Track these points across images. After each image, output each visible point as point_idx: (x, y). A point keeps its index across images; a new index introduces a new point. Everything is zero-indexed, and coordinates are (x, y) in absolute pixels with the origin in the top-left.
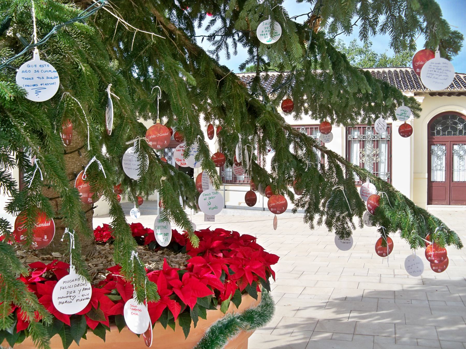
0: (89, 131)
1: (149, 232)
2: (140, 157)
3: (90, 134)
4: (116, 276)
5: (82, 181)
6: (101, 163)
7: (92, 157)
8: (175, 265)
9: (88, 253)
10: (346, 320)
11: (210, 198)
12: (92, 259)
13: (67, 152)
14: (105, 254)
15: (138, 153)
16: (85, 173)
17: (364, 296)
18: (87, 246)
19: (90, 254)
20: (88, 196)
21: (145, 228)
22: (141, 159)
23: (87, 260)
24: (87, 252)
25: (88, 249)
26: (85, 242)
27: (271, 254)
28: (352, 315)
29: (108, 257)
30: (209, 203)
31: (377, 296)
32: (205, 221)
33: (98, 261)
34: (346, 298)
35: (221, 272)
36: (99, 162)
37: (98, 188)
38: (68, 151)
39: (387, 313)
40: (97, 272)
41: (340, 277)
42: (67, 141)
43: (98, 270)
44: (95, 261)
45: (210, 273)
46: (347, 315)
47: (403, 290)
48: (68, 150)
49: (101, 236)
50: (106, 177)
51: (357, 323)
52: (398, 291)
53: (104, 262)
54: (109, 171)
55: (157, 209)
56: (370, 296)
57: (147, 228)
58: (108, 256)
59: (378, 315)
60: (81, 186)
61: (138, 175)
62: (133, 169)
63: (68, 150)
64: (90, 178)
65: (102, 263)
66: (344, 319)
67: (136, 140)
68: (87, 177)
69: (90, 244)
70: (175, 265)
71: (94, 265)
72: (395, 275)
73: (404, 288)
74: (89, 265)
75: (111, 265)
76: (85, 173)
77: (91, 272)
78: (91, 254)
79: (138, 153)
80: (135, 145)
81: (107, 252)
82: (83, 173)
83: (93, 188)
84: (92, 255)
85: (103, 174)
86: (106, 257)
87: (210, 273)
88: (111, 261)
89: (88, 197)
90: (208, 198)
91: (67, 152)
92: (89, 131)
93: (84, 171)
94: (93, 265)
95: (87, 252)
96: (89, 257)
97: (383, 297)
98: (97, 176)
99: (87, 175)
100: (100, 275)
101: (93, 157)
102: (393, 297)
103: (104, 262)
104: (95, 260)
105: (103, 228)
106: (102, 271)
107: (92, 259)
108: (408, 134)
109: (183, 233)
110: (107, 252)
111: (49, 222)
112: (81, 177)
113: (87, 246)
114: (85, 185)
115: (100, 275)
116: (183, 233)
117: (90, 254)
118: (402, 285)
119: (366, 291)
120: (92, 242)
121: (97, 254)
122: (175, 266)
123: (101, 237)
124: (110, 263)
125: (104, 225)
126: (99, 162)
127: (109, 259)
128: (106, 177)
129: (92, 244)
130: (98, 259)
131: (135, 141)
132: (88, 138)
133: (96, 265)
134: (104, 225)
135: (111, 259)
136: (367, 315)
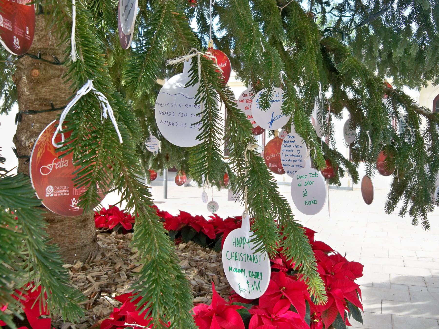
0: (74, 8)
1: (166, 217)
2: (202, 95)
3: (77, 17)
4: (132, 326)
5: (52, 151)
6: (108, 99)
7: (82, 83)
8: (212, 274)
9: (87, 255)
10: (379, 313)
11: (306, 184)
12: (91, 266)
13: (55, 108)
14: (111, 257)
15: (198, 84)
16: (60, 127)
17: (391, 282)
18: (85, 246)
19: (89, 257)
20: (71, 192)
21: (161, 211)
22: (203, 99)
23: (84, 269)
24: (85, 254)
25: (86, 250)
26: (83, 241)
27: (353, 262)
28: (384, 305)
29: (115, 264)
30: (305, 193)
31: (406, 283)
32: (229, 200)
33: (100, 271)
34: (372, 284)
35: (305, 306)
36: (102, 98)
37: (99, 173)
38: (58, 105)
39: (423, 305)
40: (99, 290)
41: (360, 258)
42: (16, 41)
43: (100, 287)
44: (96, 272)
45: (287, 308)
46: (379, 306)
47: (433, 276)
48: (57, 104)
49: (106, 222)
50: (121, 141)
51: (393, 317)
52: (428, 277)
53: (109, 273)
54: (126, 123)
55: (163, 180)
56: (399, 283)
57: (163, 211)
58: (115, 261)
59: (414, 306)
60: (50, 167)
61: (197, 138)
62: (180, 124)
63: (57, 104)
64: (75, 142)
65: (106, 274)
66: (376, 310)
67: (189, 57)
68: (65, 138)
69: (88, 243)
70: (212, 274)
71: (95, 278)
72: (418, 258)
73: (434, 274)
74: (88, 277)
75: (120, 276)
76: (60, 127)
77: (90, 291)
78: (91, 257)
79: (198, 84)
80: (187, 67)
81: (114, 254)
82: (56, 125)
83: (84, 171)
84: (92, 259)
85: (115, 131)
86: (113, 263)
87: (287, 308)
88: (120, 270)
89: (71, 196)
90: (303, 184)
91: (55, 108)
92: (74, 8)
93: (58, 120)
94: (93, 277)
95: (85, 254)
96: (88, 264)
97: (413, 284)
98: (96, 137)
99: (67, 134)
100: (103, 296)
101: (86, 82)
102: (424, 284)
103: (109, 273)
104: (96, 269)
105: (108, 210)
106: (106, 289)
107: (91, 266)
108: (258, 131)
109: (211, 219)
110: (114, 254)
111: (225, 63)
112: (50, 139)
113: (85, 246)
114: (63, 164)
115: (103, 296)
116: (211, 219)
117: (89, 257)
118: (430, 270)
119: (393, 277)
120: (92, 240)
121: (99, 258)
122: (212, 276)
123: (106, 222)
124: (119, 274)
125: (110, 206)
126: (102, 98)
127: (117, 267)
128: (121, 141)
129: (92, 242)
130: (101, 267)
131: (187, 59)
132: (70, 31)
133: (98, 278)
134: (110, 206)
135: (120, 267)
136: (401, 307)
